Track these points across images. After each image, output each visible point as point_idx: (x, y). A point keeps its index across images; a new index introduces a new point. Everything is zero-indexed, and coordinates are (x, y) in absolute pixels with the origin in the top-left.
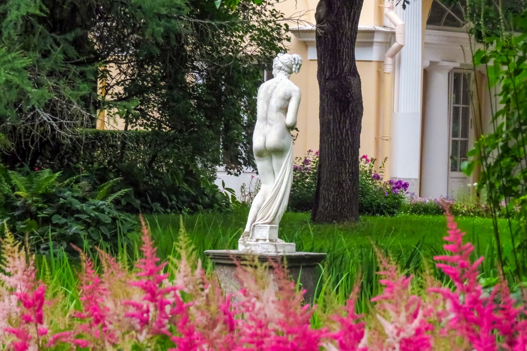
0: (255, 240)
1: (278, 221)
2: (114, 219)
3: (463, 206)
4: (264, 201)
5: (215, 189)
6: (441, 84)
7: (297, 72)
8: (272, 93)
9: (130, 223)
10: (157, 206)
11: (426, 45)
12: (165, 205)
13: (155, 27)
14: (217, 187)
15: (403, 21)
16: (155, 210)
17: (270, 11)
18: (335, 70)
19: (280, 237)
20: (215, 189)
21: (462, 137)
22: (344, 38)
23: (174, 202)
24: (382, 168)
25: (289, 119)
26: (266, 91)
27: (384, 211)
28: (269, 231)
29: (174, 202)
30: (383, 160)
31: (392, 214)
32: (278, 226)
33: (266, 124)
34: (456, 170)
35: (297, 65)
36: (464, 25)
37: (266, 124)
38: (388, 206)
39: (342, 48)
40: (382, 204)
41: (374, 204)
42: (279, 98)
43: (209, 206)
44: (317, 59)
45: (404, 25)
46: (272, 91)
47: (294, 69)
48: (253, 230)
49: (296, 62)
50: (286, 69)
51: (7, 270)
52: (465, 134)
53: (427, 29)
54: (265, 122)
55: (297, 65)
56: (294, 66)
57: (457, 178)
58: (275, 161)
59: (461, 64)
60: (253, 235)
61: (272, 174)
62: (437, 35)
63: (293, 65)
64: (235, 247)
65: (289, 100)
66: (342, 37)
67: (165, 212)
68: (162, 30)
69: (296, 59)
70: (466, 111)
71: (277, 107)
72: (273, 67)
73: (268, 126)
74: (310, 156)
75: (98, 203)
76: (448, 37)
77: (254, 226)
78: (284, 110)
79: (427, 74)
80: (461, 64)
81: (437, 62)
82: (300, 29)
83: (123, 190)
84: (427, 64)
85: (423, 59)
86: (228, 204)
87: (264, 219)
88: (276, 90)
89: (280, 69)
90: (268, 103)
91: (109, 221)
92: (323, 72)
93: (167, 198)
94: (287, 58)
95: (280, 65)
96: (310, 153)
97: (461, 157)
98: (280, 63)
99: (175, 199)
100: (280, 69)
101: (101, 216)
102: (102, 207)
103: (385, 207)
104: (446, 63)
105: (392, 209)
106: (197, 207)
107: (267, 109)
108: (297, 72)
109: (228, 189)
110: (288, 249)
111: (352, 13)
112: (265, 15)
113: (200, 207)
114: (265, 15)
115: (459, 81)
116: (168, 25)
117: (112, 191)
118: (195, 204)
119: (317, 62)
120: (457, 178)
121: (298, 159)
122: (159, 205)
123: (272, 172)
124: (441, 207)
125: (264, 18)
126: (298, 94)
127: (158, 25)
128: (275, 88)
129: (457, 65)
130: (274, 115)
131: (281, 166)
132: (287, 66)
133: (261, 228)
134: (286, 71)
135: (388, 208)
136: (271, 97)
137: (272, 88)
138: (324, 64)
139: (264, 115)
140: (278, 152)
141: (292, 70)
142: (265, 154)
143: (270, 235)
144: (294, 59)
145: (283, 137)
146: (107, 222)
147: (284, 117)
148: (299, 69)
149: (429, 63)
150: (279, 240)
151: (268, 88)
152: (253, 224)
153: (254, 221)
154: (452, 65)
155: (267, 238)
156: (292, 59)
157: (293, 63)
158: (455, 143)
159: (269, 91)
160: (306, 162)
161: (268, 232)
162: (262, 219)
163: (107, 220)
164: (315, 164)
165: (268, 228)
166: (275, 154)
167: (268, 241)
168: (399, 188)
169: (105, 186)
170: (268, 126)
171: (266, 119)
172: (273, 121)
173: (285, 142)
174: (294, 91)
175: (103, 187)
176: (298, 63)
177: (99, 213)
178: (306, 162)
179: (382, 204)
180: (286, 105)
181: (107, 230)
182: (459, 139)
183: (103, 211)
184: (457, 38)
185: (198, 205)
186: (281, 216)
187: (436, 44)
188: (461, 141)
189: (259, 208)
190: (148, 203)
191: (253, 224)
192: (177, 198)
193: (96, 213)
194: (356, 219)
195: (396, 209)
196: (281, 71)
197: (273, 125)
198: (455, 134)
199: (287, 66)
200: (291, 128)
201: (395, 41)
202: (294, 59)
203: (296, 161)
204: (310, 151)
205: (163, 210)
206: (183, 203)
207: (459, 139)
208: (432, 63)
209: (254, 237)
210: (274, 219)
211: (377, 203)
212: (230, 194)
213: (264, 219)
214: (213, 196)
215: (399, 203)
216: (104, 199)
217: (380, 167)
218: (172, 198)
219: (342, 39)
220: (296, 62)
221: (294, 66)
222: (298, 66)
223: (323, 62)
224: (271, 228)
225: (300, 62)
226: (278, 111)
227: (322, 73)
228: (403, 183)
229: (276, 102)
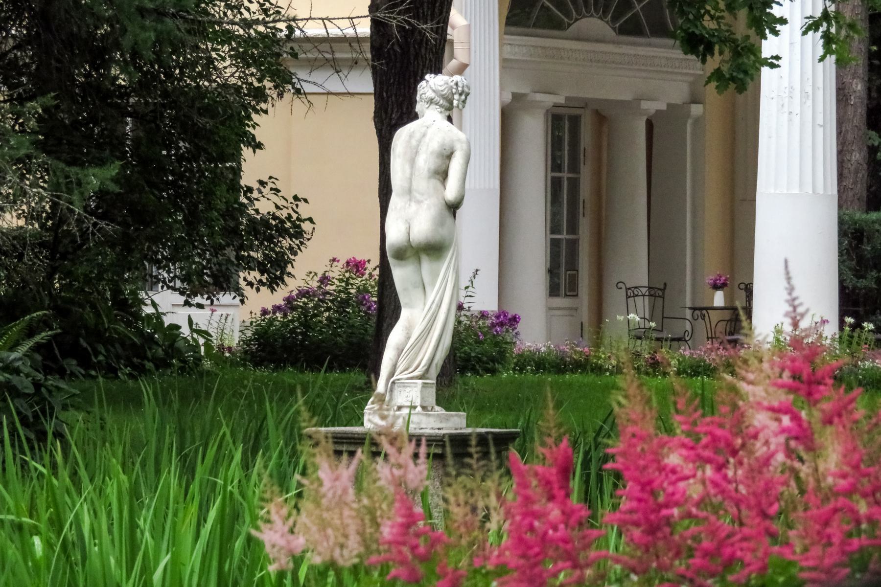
0: (396, 408)
1: (434, 372)
2: (37, 385)
3: (609, 357)
4: (408, 338)
5: (175, 332)
6: (533, 134)
7: (461, 106)
8: (418, 146)
9: (67, 392)
10: (72, 364)
11: (506, 64)
12: (85, 362)
13: (138, 31)
14: (180, 327)
15: (466, 18)
16: (68, 372)
17: (258, 2)
18: (407, 108)
19: (438, 403)
20: (175, 332)
21: (568, 233)
22: (423, 51)
23: (101, 358)
24: (470, 289)
25: (451, 192)
26: (409, 142)
27: (477, 367)
28: (421, 392)
29: (101, 358)
30: (472, 275)
31: (493, 371)
32: (434, 382)
33: (410, 200)
34: (558, 295)
35: (461, 95)
36: (569, 25)
37: (410, 200)
38: (485, 359)
39: (421, 67)
40: (473, 355)
41: (458, 355)
42: (432, 153)
43: (162, 364)
44: (371, 89)
45: (469, 26)
46: (420, 141)
47: (455, 103)
48: (391, 391)
49: (460, 89)
50: (441, 102)
51: (751, 376)
52: (573, 228)
53: (506, 33)
54: (408, 197)
55: (461, 95)
56: (456, 97)
57: (559, 309)
58: (426, 265)
59: (567, 99)
60: (391, 399)
61: (420, 290)
62: (526, 44)
63: (453, 94)
64: (358, 420)
65: (449, 156)
66: (420, 48)
67: (88, 376)
68: (153, 36)
69: (460, 84)
70: (574, 185)
71: (429, 170)
72: (418, 98)
73: (413, 204)
74: (334, 269)
75: (9, 357)
76: (543, 48)
77: (393, 383)
78: (442, 175)
79: (508, 117)
80: (567, 99)
81: (524, 95)
82: (331, 36)
83: (43, 334)
84: (508, 98)
85: (502, 89)
86: (198, 359)
87: (410, 370)
88: (427, 139)
89: (431, 101)
90: (412, 162)
91: (31, 390)
92: (386, 113)
93: (89, 349)
94: (442, 83)
95: (430, 94)
96: (335, 263)
97: (567, 270)
98: (430, 91)
99: (103, 351)
100: (431, 101)
101: (15, 380)
102: (17, 364)
103: (479, 360)
104: (539, 97)
105: (491, 364)
106: (144, 366)
107: (411, 174)
108: (461, 106)
109: (200, 332)
110: (454, 423)
111: (437, 5)
112: (248, 10)
113: (149, 365)
114: (248, 10)
115: (564, 128)
116: (159, 27)
117: (30, 332)
118: (139, 361)
119: (373, 97)
120: (559, 309)
121: (312, 275)
122: (74, 362)
123: (421, 286)
124: (568, 359)
125: (246, 15)
126: (465, 146)
127: (143, 28)
128: (424, 135)
129: (561, 100)
130: (423, 183)
131: (438, 275)
132: (443, 97)
133: (405, 386)
134: (441, 106)
135: (484, 363)
136: (417, 152)
137: (418, 136)
138: (388, 97)
139: (406, 185)
140: (434, 249)
141: (451, 103)
142: (409, 254)
143: (422, 399)
144: (457, 84)
145: (440, 222)
146: (27, 391)
147: (442, 187)
148: (464, 102)
149: (510, 97)
150: (437, 408)
151: (411, 136)
152: (392, 380)
153: (392, 374)
154: (549, 100)
155: (418, 402)
156: (453, 84)
157: (454, 91)
158: (555, 245)
159: (414, 142)
160: (324, 280)
161: (419, 394)
162: (406, 369)
163: (26, 388)
164: (343, 284)
165: (420, 386)
166: (428, 255)
167: (419, 409)
168: (502, 324)
169: (14, 326)
170: (413, 204)
171: (409, 191)
172: (423, 194)
173: (444, 232)
174: (459, 140)
175: (12, 327)
176: (463, 91)
177: (11, 374)
178: (324, 280)
179: (473, 355)
180: (444, 167)
181: (26, 406)
182: (564, 236)
183: (17, 371)
184: (558, 49)
185: (146, 362)
186: (441, 363)
187: (524, 61)
188: (567, 240)
189: (400, 351)
190: (54, 359)
191: (392, 380)
192: (107, 350)
193: (7, 375)
194: (450, 381)
195: (499, 363)
196: (433, 106)
197: (422, 202)
198: (554, 228)
199: (443, 97)
200: (453, 208)
201: (452, 56)
202: (457, 84)
203: (308, 279)
204: (334, 260)
205: (83, 372)
206: (118, 357)
207: (564, 236)
208: (516, 97)
209: (393, 403)
210: (427, 371)
211: (465, 352)
212: (201, 341)
213: (410, 370)
214: (172, 346)
215: (502, 353)
216: (12, 349)
217: (467, 288)
218: (99, 349)
219: (420, 50)
220: (460, 89)
221: (456, 97)
222: (463, 97)
223: (385, 94)
224: (425, 385)
225: (466, 90)
226: (430, 178)
227: (384, 116)
228: (510, 316)
229: (425, 162)
